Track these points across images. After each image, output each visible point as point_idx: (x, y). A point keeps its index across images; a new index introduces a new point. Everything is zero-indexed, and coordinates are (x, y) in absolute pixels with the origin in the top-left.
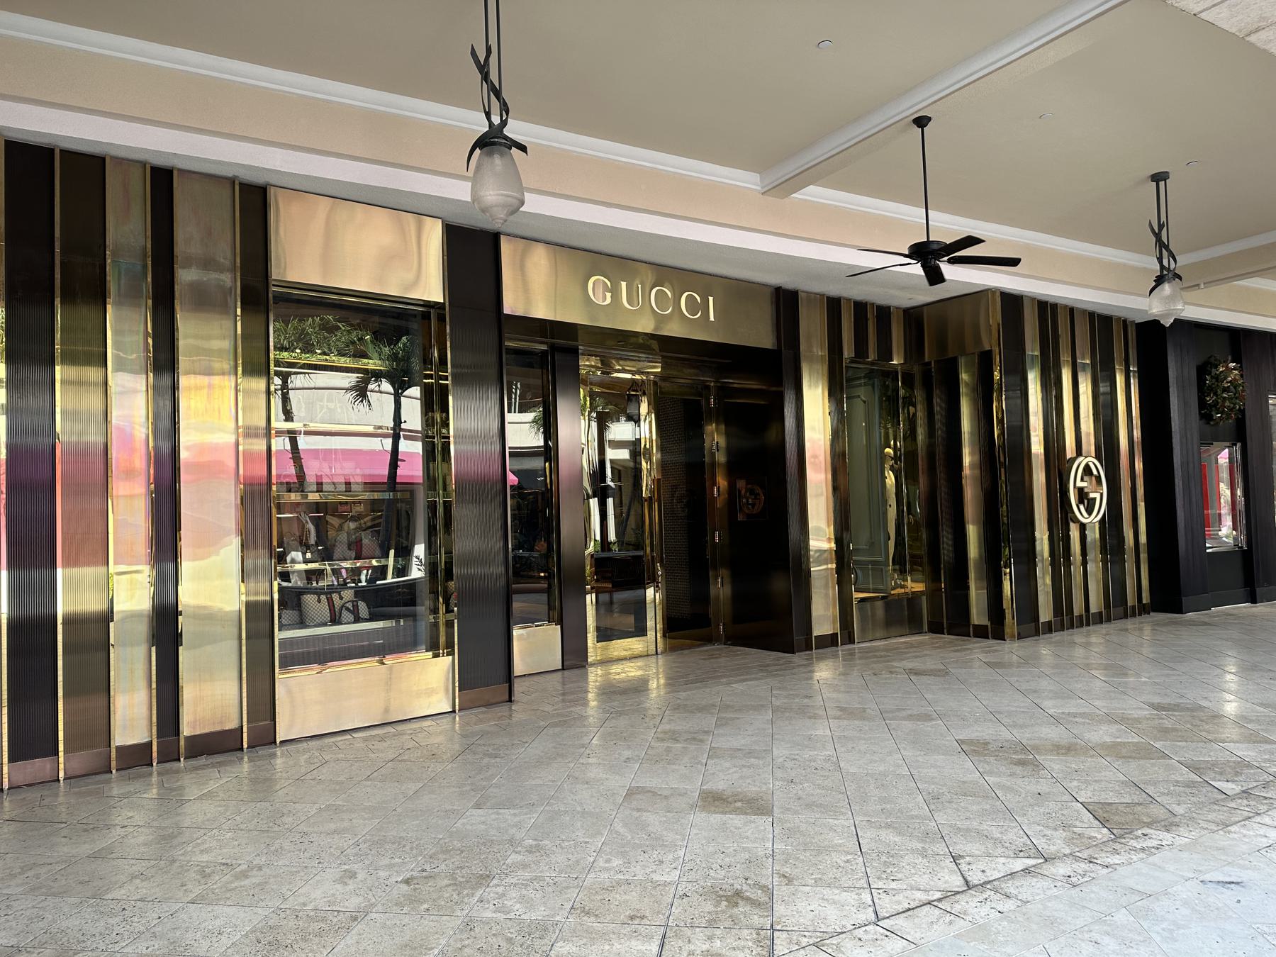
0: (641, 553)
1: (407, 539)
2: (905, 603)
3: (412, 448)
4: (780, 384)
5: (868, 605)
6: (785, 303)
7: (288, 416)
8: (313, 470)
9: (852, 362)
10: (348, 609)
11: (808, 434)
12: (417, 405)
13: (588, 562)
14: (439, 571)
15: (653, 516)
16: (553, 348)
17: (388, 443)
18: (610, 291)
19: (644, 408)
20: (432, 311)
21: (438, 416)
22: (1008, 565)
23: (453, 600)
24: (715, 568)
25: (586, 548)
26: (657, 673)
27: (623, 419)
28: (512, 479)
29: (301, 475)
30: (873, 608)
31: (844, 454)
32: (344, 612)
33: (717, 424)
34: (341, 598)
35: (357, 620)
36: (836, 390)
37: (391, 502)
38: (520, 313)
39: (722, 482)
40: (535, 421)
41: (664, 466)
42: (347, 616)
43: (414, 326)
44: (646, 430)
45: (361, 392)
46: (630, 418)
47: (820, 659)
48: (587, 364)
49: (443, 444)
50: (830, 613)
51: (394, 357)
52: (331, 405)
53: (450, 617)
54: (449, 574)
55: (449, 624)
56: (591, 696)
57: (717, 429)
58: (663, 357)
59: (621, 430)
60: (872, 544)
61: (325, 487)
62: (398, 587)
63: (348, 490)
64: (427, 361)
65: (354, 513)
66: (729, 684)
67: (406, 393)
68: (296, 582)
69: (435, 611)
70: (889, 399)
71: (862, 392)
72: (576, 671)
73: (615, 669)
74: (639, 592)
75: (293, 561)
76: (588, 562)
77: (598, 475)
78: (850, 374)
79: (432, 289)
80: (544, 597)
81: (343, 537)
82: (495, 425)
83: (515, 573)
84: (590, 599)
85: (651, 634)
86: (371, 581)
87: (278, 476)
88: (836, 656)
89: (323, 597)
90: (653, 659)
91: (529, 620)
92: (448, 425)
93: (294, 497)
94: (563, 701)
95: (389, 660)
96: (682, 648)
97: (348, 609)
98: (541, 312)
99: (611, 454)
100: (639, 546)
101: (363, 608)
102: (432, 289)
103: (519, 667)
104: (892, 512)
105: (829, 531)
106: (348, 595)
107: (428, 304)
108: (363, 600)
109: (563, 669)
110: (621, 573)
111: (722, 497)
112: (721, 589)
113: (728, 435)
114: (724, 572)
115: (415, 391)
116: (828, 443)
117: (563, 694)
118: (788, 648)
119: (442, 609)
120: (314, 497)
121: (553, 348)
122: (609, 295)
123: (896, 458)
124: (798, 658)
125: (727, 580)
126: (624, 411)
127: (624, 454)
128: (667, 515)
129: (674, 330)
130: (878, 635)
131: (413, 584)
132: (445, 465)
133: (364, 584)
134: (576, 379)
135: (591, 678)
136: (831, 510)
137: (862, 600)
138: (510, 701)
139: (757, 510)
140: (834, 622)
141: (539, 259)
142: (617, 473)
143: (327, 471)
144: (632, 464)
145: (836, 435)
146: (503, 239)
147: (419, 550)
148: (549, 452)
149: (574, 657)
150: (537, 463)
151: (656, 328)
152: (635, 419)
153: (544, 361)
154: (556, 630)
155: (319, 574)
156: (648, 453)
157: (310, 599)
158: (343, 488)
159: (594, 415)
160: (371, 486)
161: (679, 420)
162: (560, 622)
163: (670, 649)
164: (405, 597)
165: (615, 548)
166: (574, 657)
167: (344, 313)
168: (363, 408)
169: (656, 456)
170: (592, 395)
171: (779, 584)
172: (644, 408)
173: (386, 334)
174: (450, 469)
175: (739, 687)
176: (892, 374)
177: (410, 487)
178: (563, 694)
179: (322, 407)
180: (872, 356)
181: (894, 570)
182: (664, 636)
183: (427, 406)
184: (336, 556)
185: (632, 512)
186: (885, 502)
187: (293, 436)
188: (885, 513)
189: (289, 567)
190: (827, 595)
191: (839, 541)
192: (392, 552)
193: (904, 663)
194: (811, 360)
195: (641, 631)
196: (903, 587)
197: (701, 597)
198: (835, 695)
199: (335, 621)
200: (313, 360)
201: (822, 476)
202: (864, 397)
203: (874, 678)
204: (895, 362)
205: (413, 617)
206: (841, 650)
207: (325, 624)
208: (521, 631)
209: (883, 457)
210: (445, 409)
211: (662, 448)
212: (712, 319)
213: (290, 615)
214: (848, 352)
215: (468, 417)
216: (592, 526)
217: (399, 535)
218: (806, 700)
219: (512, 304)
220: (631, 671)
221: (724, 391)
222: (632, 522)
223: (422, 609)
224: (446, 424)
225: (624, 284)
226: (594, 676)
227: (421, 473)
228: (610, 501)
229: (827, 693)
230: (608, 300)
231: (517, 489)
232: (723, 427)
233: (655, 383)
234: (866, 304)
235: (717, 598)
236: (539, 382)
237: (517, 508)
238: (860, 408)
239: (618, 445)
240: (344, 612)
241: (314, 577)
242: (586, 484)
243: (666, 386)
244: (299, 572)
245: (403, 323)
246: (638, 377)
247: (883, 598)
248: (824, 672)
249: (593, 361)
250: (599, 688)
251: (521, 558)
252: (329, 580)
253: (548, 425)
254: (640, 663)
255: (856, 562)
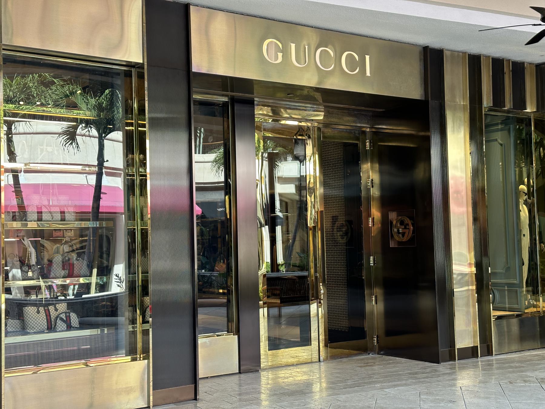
0: (305, 273)
1: (108, 260)
2: (537, 320)
3: (114, 183)
4: (427, 129)
5: (504, 322)
6: (432, 60)
7: (12, 155)
8: (33, 202)
9: (490, 110)
10: (62, 319)
11: (452, 173)
12: (120, 147)
13: (261, 280)
14: (138, 288)
15: (316, 243)
16: (233, 100)
17: (92, 180)
18: (282, 52)
19: (309, 149)
20: (133, 70)
21: (137, 157)
22: (149, 219)
23: (148, 313)
24: (370, 287)
25: (259, 268)
26: (320, 378)
27: (290, 158)
28: (197, 210)
29: (22, 207)
30: (508, 326)
31: (483, 190)
32: (59, 322)
33: (372, 162)
34: (56, 310)
35: (70, 327)
36: (477, 131)
37: (95, 229)
38: (204, 71)
39: (376, 213)
40: (215, 161)
41: (326, 199)
42: (61, 325)
43: (118, 81)
44: (311, 168)
45: (71, 136)
46: (296, 158)
47: (462, 368)
48: (261, 113)
49: (141, 180)
50: (471, 328)
51: (99, 108)
52: (49, 149)
53: (146, 327)
54: (145, 291)
55: (145, 333)
56: (263, 396)
57: (372, 168)
58: (325, 107)
59: (288, 168)
60: (508, 269)
61: (45, 217)
62: (103, 300)
63: (63, 219)
64: (128, 110)
65: (68, 239)
66: (382, 388)
67: (109, 136)
68: (17, 295)
69: (133, 321)
70: (522, 141)
71: (499, 136)
72: (251, 375)
73: (283, 373)
74: (303, 307)
75: (14, 278)
76: (261, 280)
77: (270, 207)
78: (489, 120)
79: (133, 51)
80: (224, 310)
81: (58, 259)
82: (184, 163)
83: (200, 290)
84: (263, 312)
85: (314, 343)
86: (78, 295)
87: (6, 206)
88: (476, 366)
89: (41, 309)
90: (316, 366)
91: (212, 330)
92: (145, 165)
93: (16, 225)
94: (240, 400)
95: (94, 363)
96: (341, 356)
97: (62, 319)
98: (221, 70)
99: (280, 189)
100: (304, 267)
101: (74, 319)
102: (133, 51)
103: (201, 373)
104: (526, 242)
105: (471, 257)
106: (62, 307)
107: (130, 65)
108: (74, 311)
109: (240, 373)
110: (288, 290)
111: (376, 227)
112: (375, 305)
113: (381, 172)
114: (378, 291)
115: (118, 135)
116: (469, 181)
117: (240, 395)
118: (436, 360)
119: (139, 319)
120: (32, 225)
121: (233, 100)
122: (280, 55)
123: (529, 194)
124: (443, 367)
125: (381, 298)
126: (291, 152)
127: (290, 189)
128: (330, 242)
129: (334, 83)
130: (514, 347)
131: (114, 299)
132: (142, 199)
133: (72, 297)
134: (252, 125)
135: (264, 380)
136: (475, 240)
137: (499, 318)
138: (196, 399)
139: (405, 239)
140: (474, 337)
141: (220, 26)
142: (285, 206)
143: (46, 203)
144: (297, 198)
145: (476, 173)
146: (192, 8)
147: (119, 269)
148: (229, 187)
149: (249, 362)
150: (218, 196)
151: (320, 82)
152: (301, 159)
153: (228, 110)
154: (233, 339)
155: (37, 289)
156: (313, 191)
157: (30, 311)
158: (58, 216)
159: (266, 155)
160: (81, 216)
161: (340, 159)
162: (238, 332)
163: (332, 357)
164: (109, 308)
165: (283, 269)
166: (249, 362)
167: (59, 72)
168: (72, 149)
169: (320, 191)
170: (265, 139)
171: (426, 302)
172: (309, 149)
173: (97, 89)
174: (146, 202)
175: (391, 391)
176: (525, 121)
177: (112, 217)
178: (240, 395)
179: (42, 150)
180: (508, 105)
181: (528, 291)
182: (326, 346)
183: (129, 148)
184: (52, 275)
185: (298, 238)
186: (519, 231)
187: (15, 173)
188: (520, 241)
189: (10, 283)
190: (468, 313)
191: (479, 265)
192: (95, 271)
193: (537, 373)
194: (455, 109)
195: (305, 341)
196: (535, 306)
197: (358, 313)
198: (476, 401)
199: (51, 328)
200: (34, 111)
201: (464, 209)
202: (501, 141)
203: (510, 386)
204: (528, 110)
205: (115, 325)
206: (481, 360)
207: (42, 332)
208: (204, 340)
209: (518, 193)
210: (143, 151)
211: (325, 184)
212: (368, 74)
213: (14, 323)
214: (487, 101)
215: (163, 156)
216: (259, 252)
217: (101, 257)
218: (450, 405)
219: (200, 63)
220: (297, 376)
221: (377, 135)
222: (297, 248)
223: (123, 319)
224: (143, 164)
225: (293, 46)
226: (266, 379)
227: (122, 204)
228: (279, 229)
229: (469, 399)
230: (280, 59)
231: (202, 217)
232: (377, 166)
233: (319, 129)
234: (503, 60)
235: (372, 313)
236: (220, 128)
237: (201, 234)
238: (496, 150)
239: (286, 180)
240: (59, 322)
241: (33, 292)
242: (260, 214)
243: (328, 132)
244: (19, 288)
245: (109, 80)
246: (303, 124)
247: (518, 316)
248: (466, 379)
249: (266, 111)
250: (270, 390)
251: (203, 276)
252: (45, 295)
253: (228, 163)
254: (305, 368)
255: (495, 285)
